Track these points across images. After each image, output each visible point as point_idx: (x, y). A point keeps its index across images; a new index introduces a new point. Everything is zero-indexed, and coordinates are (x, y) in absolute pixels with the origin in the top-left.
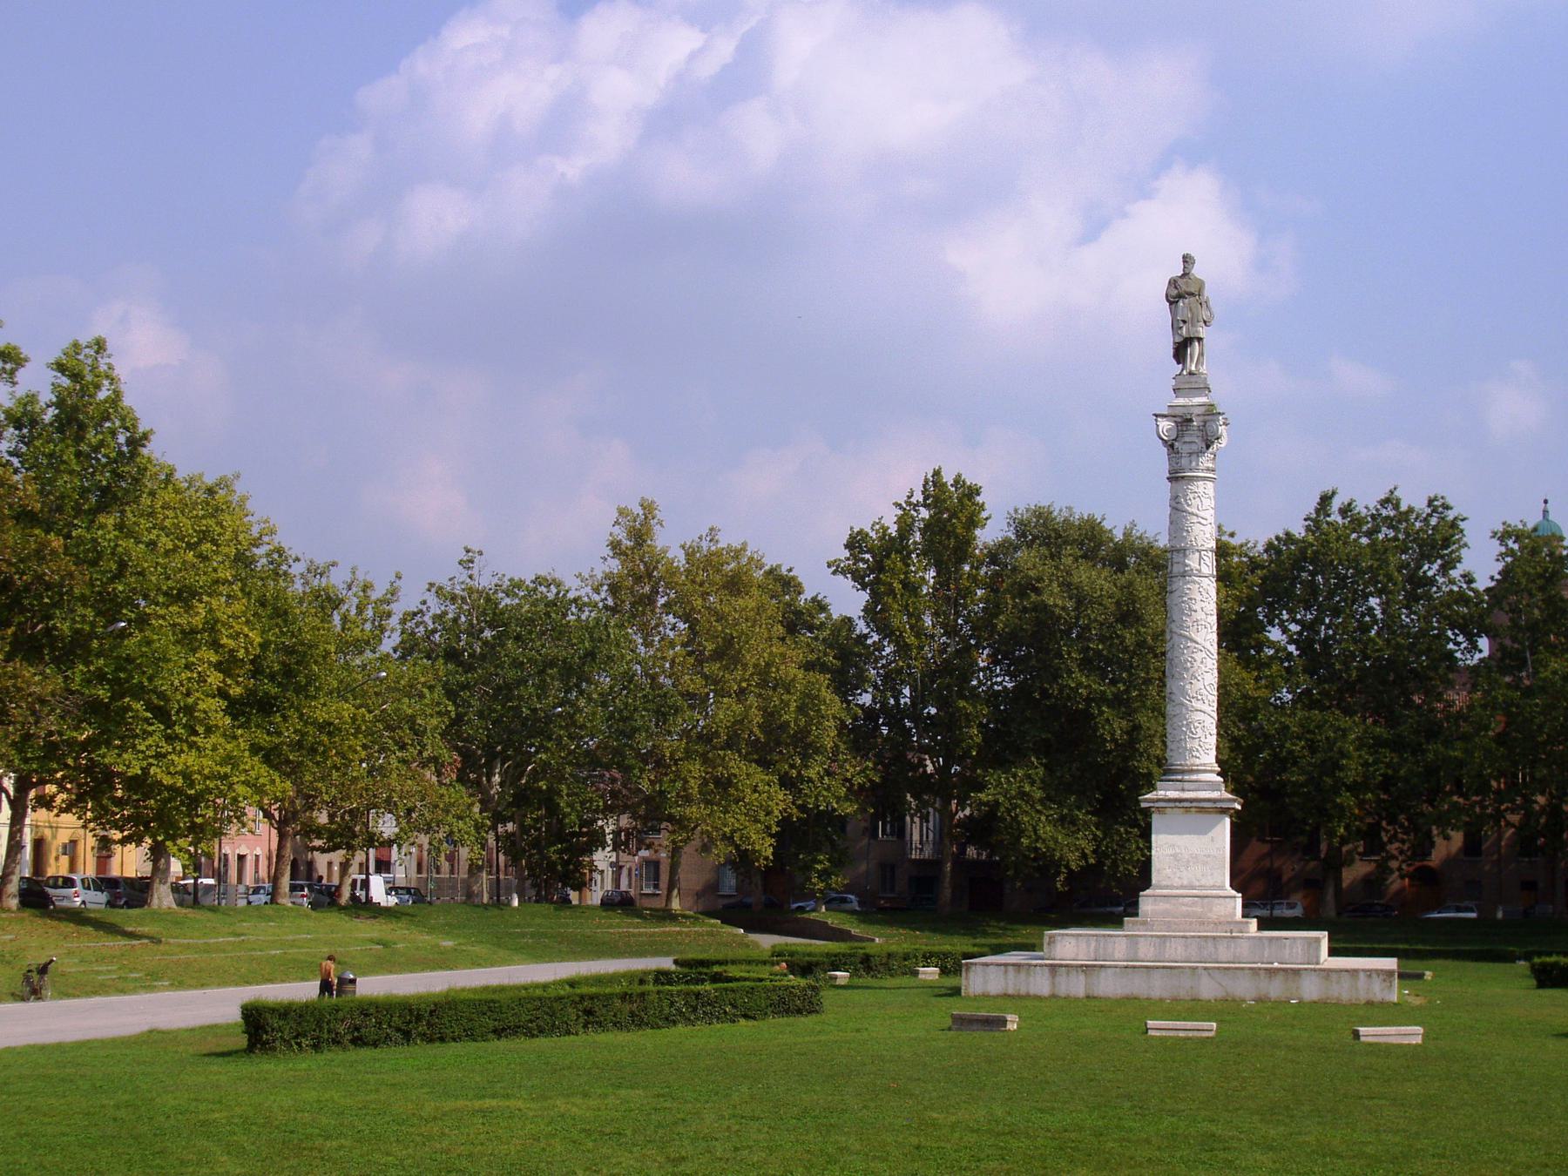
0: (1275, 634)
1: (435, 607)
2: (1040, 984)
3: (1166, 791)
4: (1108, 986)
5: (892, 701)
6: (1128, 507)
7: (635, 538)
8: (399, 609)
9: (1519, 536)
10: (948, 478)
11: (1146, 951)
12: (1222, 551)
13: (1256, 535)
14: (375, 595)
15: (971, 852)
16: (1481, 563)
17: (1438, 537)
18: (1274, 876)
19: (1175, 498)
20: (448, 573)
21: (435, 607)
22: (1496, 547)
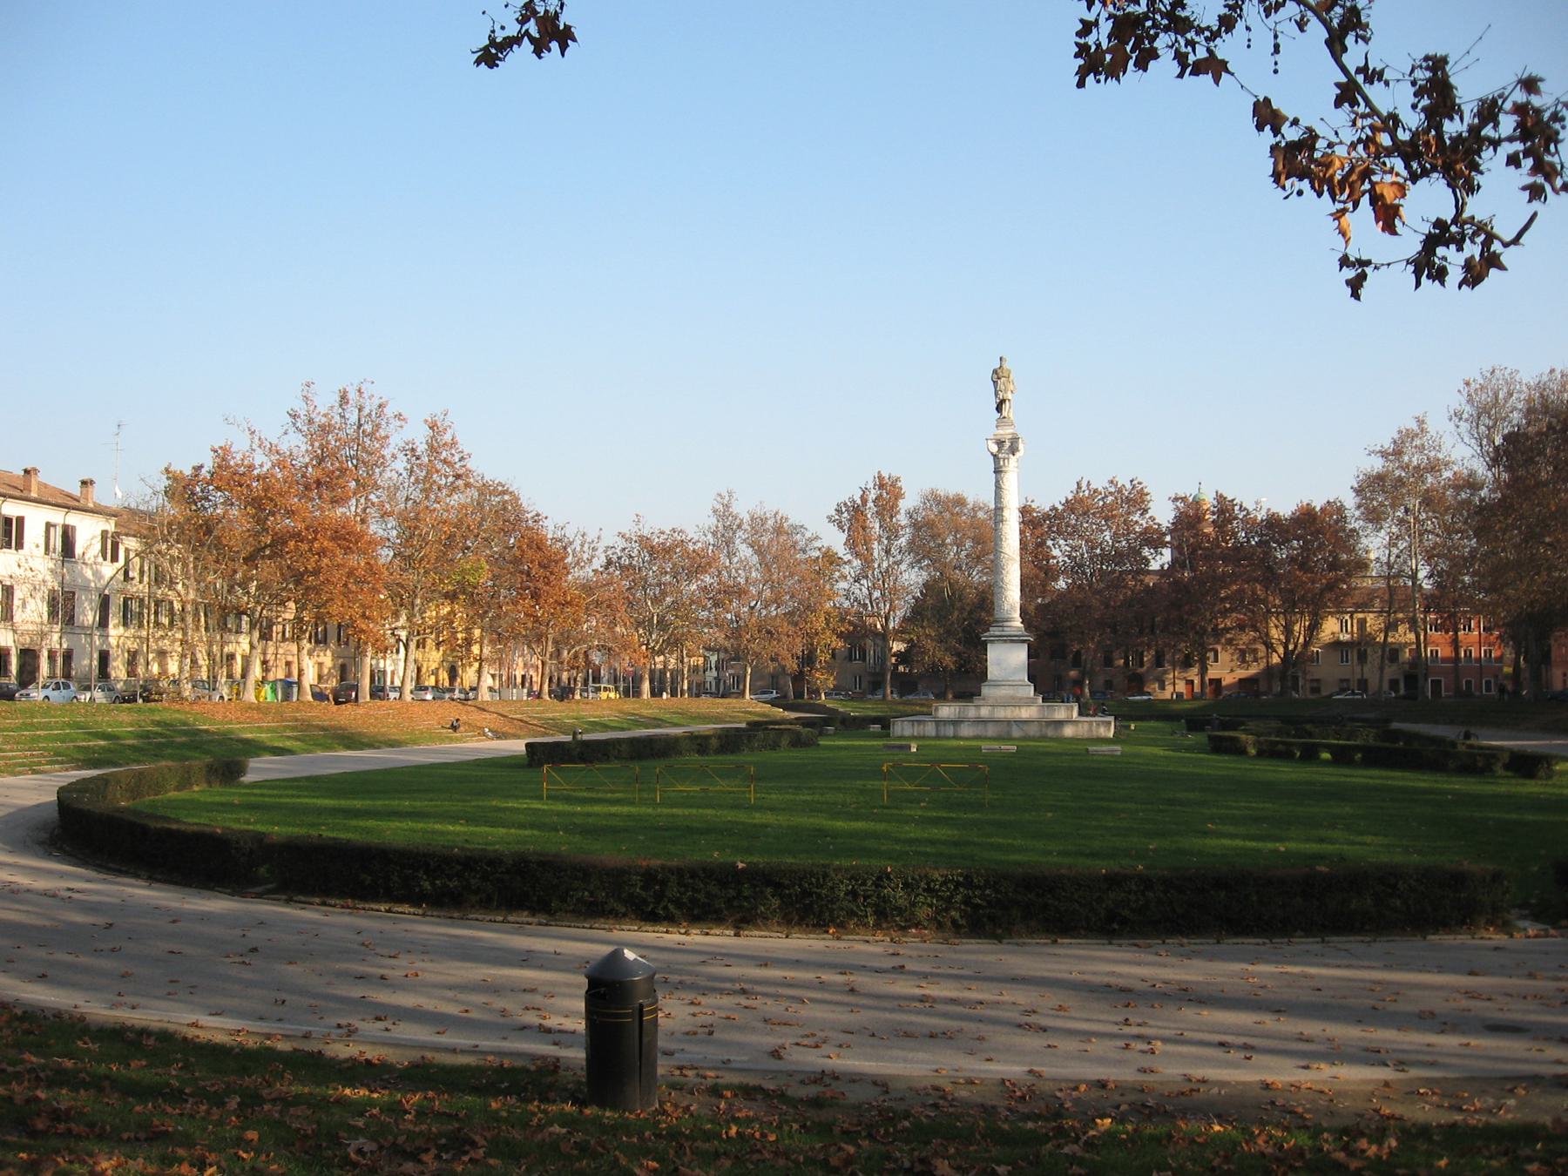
0: (1056, 552)
1: (621, 543)
2: (930, 729)
3: (994, 631)
4: (966, 731)
5: (1547, 540)
6: (978, 492)
7: (724, 512)
8: (601, 547)
9: (1183, 499)
10: (885, 475)
11: (985, 712)
12: (1025, 511)
13: (1050, 498)
14: (421, 448)
15: (901, 668)
16: (1163, 514)
17: (1137, 499)
18: (1048, 677)
19: (997, 482)
20: (629, 528)
21: (621, 543)
22: (1171, 506)
